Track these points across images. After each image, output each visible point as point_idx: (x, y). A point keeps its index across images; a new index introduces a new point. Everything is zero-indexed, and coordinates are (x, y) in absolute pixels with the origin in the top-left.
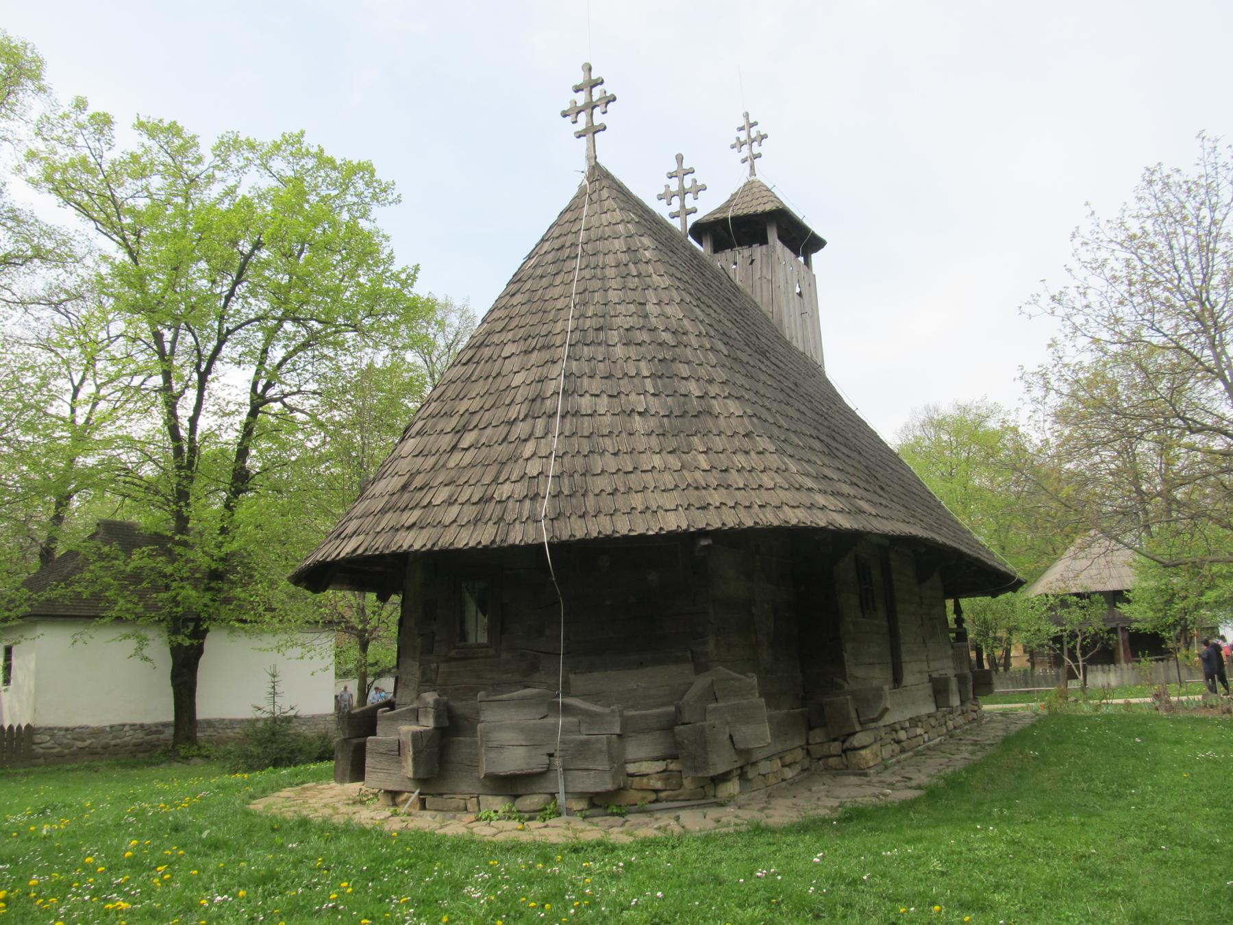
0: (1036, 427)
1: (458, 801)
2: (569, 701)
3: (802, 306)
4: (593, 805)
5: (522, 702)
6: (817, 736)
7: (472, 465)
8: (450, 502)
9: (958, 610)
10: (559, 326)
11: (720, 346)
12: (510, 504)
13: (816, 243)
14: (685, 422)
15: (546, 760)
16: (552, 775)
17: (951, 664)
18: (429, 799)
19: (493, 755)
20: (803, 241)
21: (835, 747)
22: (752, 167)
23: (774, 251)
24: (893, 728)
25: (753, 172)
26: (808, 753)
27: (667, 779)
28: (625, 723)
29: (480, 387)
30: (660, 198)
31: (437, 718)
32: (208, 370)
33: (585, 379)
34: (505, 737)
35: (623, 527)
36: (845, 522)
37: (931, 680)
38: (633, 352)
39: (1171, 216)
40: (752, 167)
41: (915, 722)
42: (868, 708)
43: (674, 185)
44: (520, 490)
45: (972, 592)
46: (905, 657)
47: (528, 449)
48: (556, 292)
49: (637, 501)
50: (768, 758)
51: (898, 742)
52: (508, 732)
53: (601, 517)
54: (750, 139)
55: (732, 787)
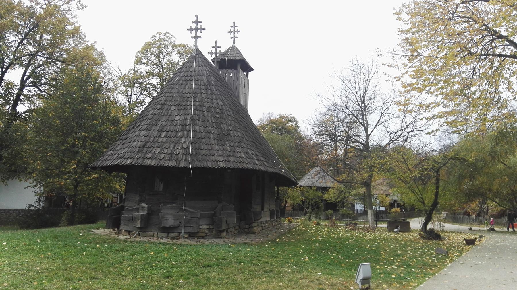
0: (307, 129)
1: (151, 234)
2: (186, 208)
3: (245, 91)
4: (190, 236)
5: (172, 208)
6: (243, 223)
7: (166, 142)
8: (161, 153)
9: (278, 189)
10: (189, 103)
11: (232, 114)
12: (179, 155)
13: (252, 70)
14: (223, 137)
15: (179, 223)
16: (180, 228)
17: (275, 206)
18: (141, 233)
19: (165, 221)
20: (247, 68)
21: (247, 226)
22: (234, 41)
23: (239, 72)
24: (261, 223)
25: (234, 43)
26: (240, 228)
27: (209, 231)
28: (201, 215)
29: (164, 118)
30: (209, 53)
31: (148, 211)
32: (6, 71)
33: (197, 121)
34: (169, 217)
35: (209, 165)
36: (263, 169)
37: (270, 210)
38: (210, 114)
39: (357, 73)
40: (234, 41)
41: (266, 222)
42: (257, 216)
43: (232, 29)
44: (182, 152)
45: (283, 185)
46: (265, 204)
47: (183, 140)
48: (187, 91)
49: (213, 158)
50: (232, 227)
51: (262, 227)
52: (169, 216)
53: (204, 162)
54: (234, 31)
55: (224, 234)
